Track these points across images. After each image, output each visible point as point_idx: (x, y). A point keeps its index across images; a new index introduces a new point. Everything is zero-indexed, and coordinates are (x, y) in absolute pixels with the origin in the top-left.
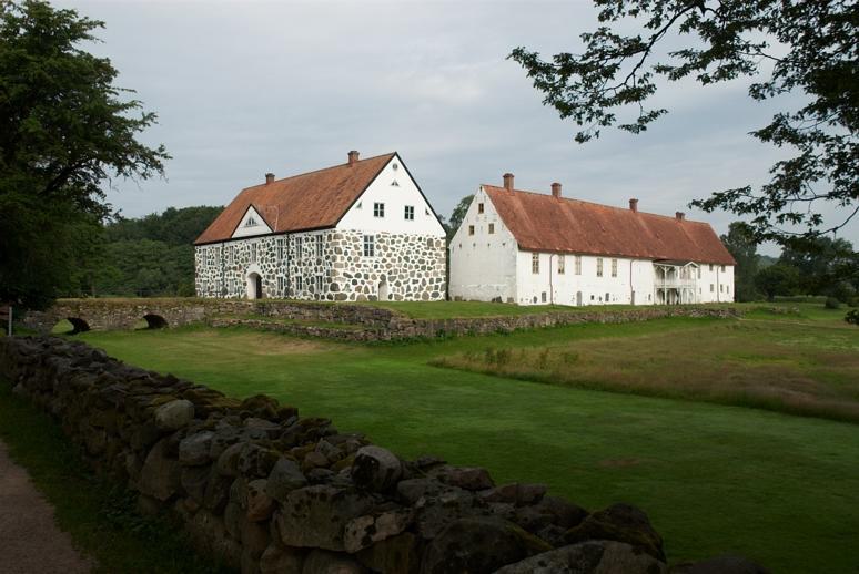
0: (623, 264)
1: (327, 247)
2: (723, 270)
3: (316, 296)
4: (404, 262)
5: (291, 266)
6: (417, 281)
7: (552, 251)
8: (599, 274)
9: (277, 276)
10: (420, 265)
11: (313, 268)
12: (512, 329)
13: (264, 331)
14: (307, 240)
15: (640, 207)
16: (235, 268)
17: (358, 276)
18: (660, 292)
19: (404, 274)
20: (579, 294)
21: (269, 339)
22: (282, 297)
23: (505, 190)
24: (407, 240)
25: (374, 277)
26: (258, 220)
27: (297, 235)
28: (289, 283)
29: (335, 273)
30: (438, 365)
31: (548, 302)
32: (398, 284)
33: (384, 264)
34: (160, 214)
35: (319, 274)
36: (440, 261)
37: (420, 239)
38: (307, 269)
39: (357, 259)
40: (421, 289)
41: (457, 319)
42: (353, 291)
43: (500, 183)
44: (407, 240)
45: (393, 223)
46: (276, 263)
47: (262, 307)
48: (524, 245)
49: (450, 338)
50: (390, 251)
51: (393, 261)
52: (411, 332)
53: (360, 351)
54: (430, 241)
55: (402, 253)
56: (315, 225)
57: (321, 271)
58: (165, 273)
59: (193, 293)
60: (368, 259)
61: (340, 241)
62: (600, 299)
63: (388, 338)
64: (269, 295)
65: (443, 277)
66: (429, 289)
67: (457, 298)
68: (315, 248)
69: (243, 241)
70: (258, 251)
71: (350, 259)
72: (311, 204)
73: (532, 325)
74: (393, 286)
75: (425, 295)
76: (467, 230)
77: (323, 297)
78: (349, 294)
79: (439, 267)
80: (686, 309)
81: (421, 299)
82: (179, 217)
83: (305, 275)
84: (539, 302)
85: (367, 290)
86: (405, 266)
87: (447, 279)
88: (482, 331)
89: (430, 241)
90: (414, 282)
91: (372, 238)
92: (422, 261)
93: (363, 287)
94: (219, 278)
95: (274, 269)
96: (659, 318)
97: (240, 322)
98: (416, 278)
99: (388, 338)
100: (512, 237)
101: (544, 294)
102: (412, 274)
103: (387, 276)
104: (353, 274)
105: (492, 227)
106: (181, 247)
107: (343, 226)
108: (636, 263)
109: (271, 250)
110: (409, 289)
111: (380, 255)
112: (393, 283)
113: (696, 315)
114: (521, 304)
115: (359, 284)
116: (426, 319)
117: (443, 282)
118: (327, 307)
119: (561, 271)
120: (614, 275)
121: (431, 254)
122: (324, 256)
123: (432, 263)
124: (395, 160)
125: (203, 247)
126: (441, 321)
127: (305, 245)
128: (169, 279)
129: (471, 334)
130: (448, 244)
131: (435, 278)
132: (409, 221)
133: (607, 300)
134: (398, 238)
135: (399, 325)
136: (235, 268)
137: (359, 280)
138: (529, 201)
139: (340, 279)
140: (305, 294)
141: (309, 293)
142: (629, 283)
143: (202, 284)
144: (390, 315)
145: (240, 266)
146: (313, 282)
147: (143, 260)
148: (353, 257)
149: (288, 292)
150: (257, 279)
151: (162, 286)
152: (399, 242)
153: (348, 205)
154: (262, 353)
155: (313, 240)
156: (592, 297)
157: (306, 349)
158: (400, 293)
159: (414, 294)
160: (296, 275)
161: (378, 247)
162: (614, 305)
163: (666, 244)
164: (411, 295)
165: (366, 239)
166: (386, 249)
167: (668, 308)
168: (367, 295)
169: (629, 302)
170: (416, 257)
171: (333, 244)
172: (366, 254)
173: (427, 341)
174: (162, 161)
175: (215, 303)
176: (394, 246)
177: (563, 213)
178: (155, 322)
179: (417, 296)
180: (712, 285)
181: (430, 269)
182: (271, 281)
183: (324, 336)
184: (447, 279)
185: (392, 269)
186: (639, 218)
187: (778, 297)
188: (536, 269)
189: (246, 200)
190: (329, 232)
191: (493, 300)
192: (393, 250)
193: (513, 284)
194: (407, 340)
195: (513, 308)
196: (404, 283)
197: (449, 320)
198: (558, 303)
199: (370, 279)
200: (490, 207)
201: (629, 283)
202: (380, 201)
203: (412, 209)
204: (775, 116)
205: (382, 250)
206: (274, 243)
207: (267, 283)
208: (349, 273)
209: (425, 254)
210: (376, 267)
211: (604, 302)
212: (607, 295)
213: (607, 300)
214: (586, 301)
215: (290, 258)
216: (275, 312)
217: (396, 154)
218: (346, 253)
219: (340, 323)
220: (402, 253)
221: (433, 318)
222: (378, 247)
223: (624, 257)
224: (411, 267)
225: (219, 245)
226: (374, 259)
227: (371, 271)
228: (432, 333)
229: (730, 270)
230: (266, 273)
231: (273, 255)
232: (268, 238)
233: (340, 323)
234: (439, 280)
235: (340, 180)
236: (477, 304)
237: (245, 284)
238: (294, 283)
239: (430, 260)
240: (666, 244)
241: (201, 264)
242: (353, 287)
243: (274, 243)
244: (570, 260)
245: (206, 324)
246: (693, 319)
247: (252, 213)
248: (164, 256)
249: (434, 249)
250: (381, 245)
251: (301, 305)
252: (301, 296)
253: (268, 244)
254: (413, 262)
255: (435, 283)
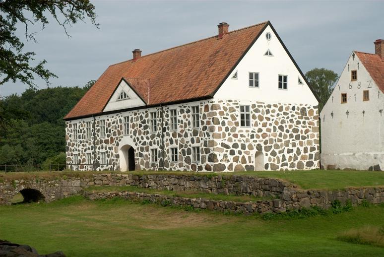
1: (204, 117)
3: (193, 167)
4: (279, 131)
5: (166, 137)
9: (150, 148)
10: (295, 135)
11: (189, 138)
13: (143, 204)
14: (182, 111)
16: (107, 142)
17: (235, 146)
19: (279, 144)
21: (151, 211)
22: (157, 169)
24: (281, 109)
25: (251, 147)
26: (131, 93)
27: (172, 107)
28: (163, 154)
29: (213, 143)
30: (351, 240)
32: (274, 154)
33: (260, 134)
34: (20, 95)
35: (196, 145)
36: (314, 130)
37: (293, 108)
38: (182, 141)
39: (234, 130)
40: (296, 158)
41: (350, 189)
42: (231, 161)
44: (281, 109)
45: (268, 93)
46: (149, 135)
47: (139, 180)
49: (346, 209)
50: (265, 121)
51: (269, 130)
52: (306, 203)
53: (255, 224)
54: (303, 110)
55: (276, 123)
56: (191, 96)
57: (198, 141)
58: (26, 149)
59: (61, 165)
60: (244, 129)
61: (218, 111)
63: (283, 211)
64: (142, 167)
65: (316, 146)
66: (303, 158)
67: (330, 167)
68: (191, 119)
69: (115, 115)
70: (130, 124)
71: (227, 129)
72: (187, 78)
74: (269, 155)
75: (300, 165)
76: (340, 98)
77: (200, 168)
78: (227, 165)
79: (313, 136)
81: (295, 168)
82: (37, 97)
83: (181, 146)
85: (244, 161)
86: (280, 135)
87: (320, 148)
89: (303, 110)
90: (290, 151)
91: (248, 108)
92: (296, 131)
93: (241, 157)
94: (91, 151)
95: (148, 141)
97: (117, 195)
98: (290, 147)
99: (283, 211)
102: (287, 144)
103: (263, 146)
104: (230, 144)
106: (40, 125)
107: (221, 96)
109: (144, 122)
110: (284, 159)
111: (256, 124)
112: (269, 153)
115: (237, 154)
116: (321, 190)
117: (317, 151)
118: (209, 178)
121: (304, 123)
122: (201, 127)
123: (307, 131)
124: (268, 29)
125: (73, 122)
127: (180, 117)
128: (29, 154)
130: (319, 111)
131: (309, 147)
132: (282, 91)
134: (273, 108)
135: (294, 196)
136: (107, 142)
137: (236, 150)
139: (218, 149)
140: (181, 165)
141: (185, 164)
143: (73, 158)
144: (281, 186)
145: (112, 139)
146: (189, 153)
147: (6, 138)
148: (230, 127)
149: (162, 163)
150: (130, 152)
151: (24, 161)
152: (274, 111)
153: (224, 75)
154: (151, 227)
155: (188, 111)
157: (193, 222)
158: (276, 163)
159: (289, 163)
160: (171, 146)
161: (254, 117)
164: (286, 164)
165: (242, 110)
166: (261, 119)
168: (244, 165)
170: (290, 126)
171: (210, 115)
172: (243, 124)
173: (322, 213)
174: (77, 19)
175: (91, 176)
176: (268, 116)
178: (31, 196)
179: (292, 165)
181: (304, 138)
182: (144, 153)
183: (211, 208)
184: (320, 148)
185: (267, 138)
189: (114, 77)
190: (205, 102)
191: (371, 168)
192: (268, 119)
194: (303, 211)
196: (280, 152)
197: (344, 191)
199: (247, 149)
200: (364, 75)
202: (254, 71)
203: (285, 78)
205: (257, 120)
206: (147, 116)
207: (141, 155)
208: (227, 143)
209: (298, 123)
210: (252, 137)
215: (164, 130)
216: (153, 184)
217: (269, 23)
218: (223, 123)
219: (224, 194)
220: (276, 123)
221: (326, 188)
222: (254, 117)
224: (285, 137)
225: (90, 120)
226: (250, 129)
227: (247, 141)
228: (326, 204)
230: (140, 145)
231: (146, 127)
232: (141, 111)
233: (224, 194)
234: (313, 149)
235: (210, 51)
236: (350, 173)
237: (118, 156)
238: (170, 155)
239: (304, 129)
241: (72, 138)
242: (231, 158)
243: (147, 116)
245: (84, 196)
247: (124, 87)
248: (25, 133)
249: (308, 119)
250: (257, 115)
251: (180, 177)
252: (177, 167)
253: (141, 117)
254: (287, 131)
255: (309, 152)
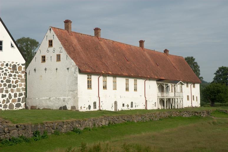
0: (140, 82)
2: (194, 87)
6: (5, 96)
7: (99, 74)
8: (127, 89)
10: (7, 84)
12: (82, 129)
15: (146, 46)
18: (162, 101)
20: (116, 103)
23: (66, 31)
31: (98, 108)
37: (7, 65)
40: (8, 101)
43: (62, 26)
48: (82, 69)
52: (15, 134)
54: (14, 67)
62: (128, 106)
65: (23, 92)
67: (33, 108)
73: (94, 125)
75: (11, 106)
76: (40, 59)
80: (181, 112)
81: (8, 108)
84: (92, 109)
88: (63, 130)
92: (8, 81)
96: (166, 118)
100: (74, 63)
101: (95, 103)
105: (59, 58)
108: (148, 83)
113: (186, 115)
114: (81, 111)
117: (23, 96)
119: (105, 87)
120: (135, 90)
121: (15, 75)
123: (16, 82)
126: (36, 125)
129: (56, 133)
131: (18, 93)
133: (132, 106)
135: (6, 129)
138: (80, 38)
142: (140, 95)
156: (123, 105)
162: (136, 110)
163: (167, 70)
167: (169, 111)
169: (144, 108)
173: (26, 140)
177: (102, 47)
180: (188, 96)
181: (14, 86)
186: (145, 53)
187: (217, 103)
188: (89, 86)
193: (75, 97)
194: (12, 140)
195: (75, 112)
197: (42, 124)
198: (104, 109)
200: (57, 43)
201: (140, 95)
204: (12, 46)
209: (10, 75)
211: (130, 108)
212: (132, 103)
213: (132, 106)
214: (120, 108)
221: (30, 123)
223: (141, 78)
228: (29, 135)
229: (198, 86)
234: (21, 95)
236: (47, 112)
239: (14, 80)
240: (167, 70)
244: (110, 80)
246: (185, 119)
255: (18, 97)
